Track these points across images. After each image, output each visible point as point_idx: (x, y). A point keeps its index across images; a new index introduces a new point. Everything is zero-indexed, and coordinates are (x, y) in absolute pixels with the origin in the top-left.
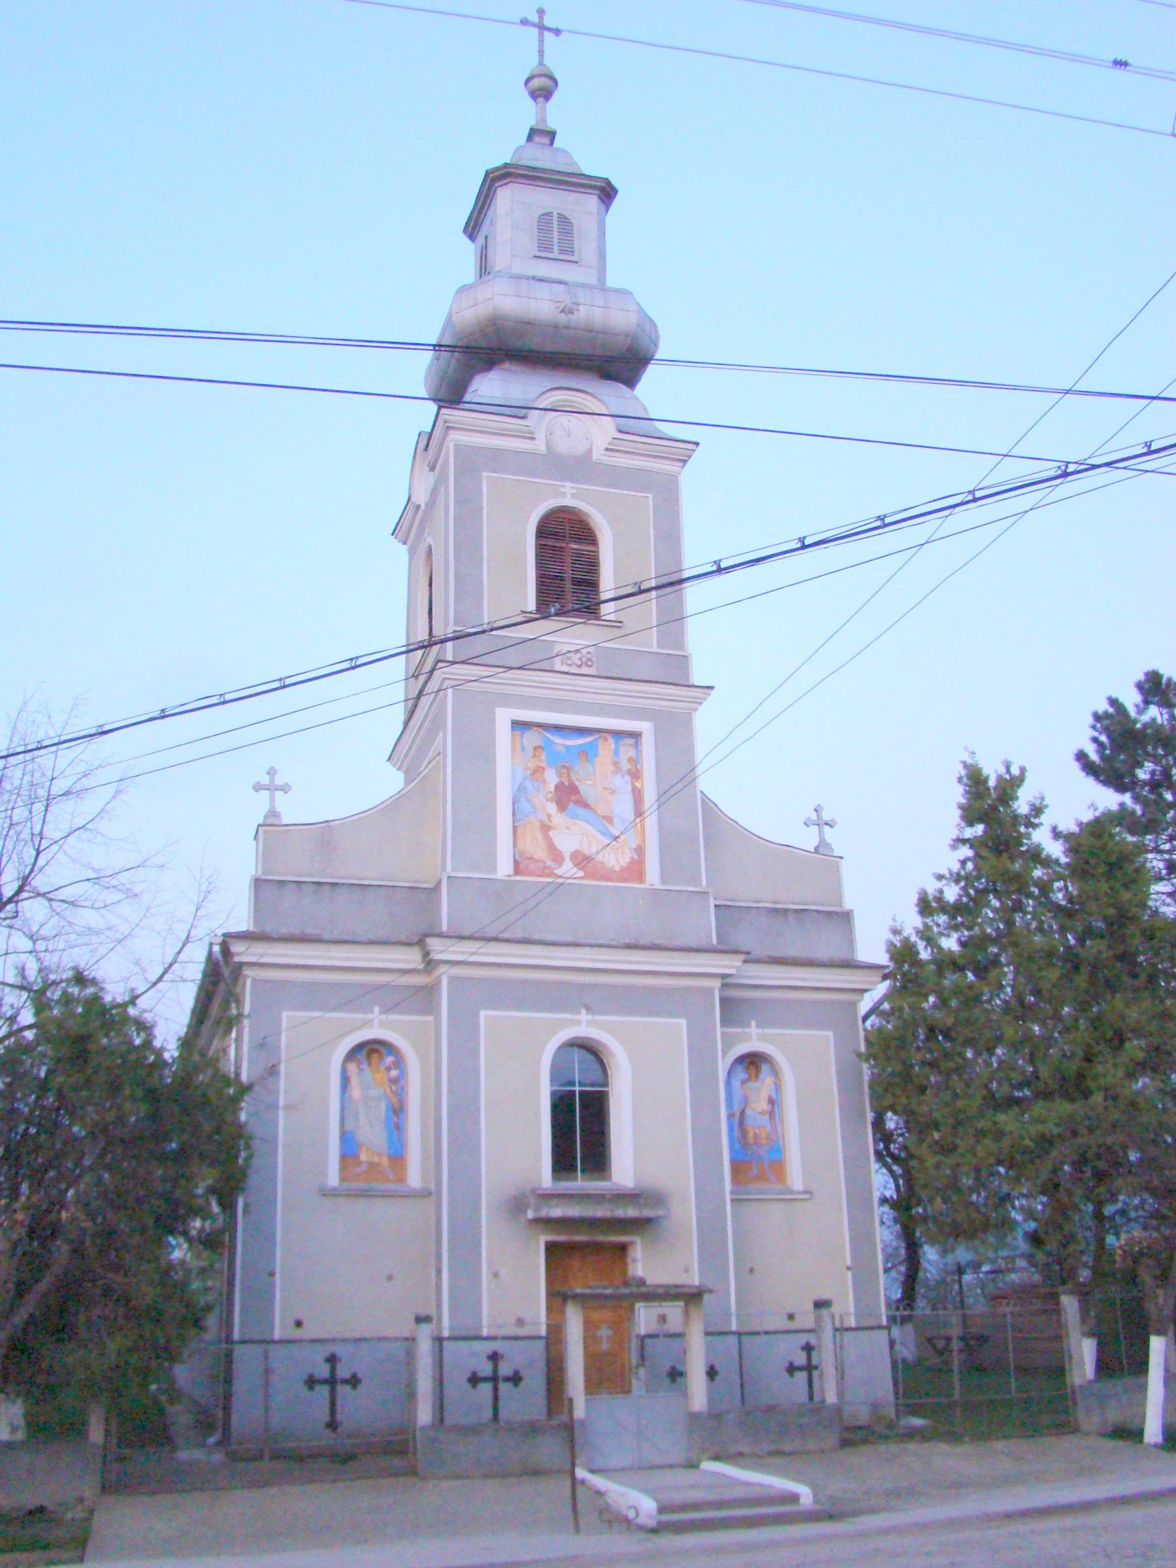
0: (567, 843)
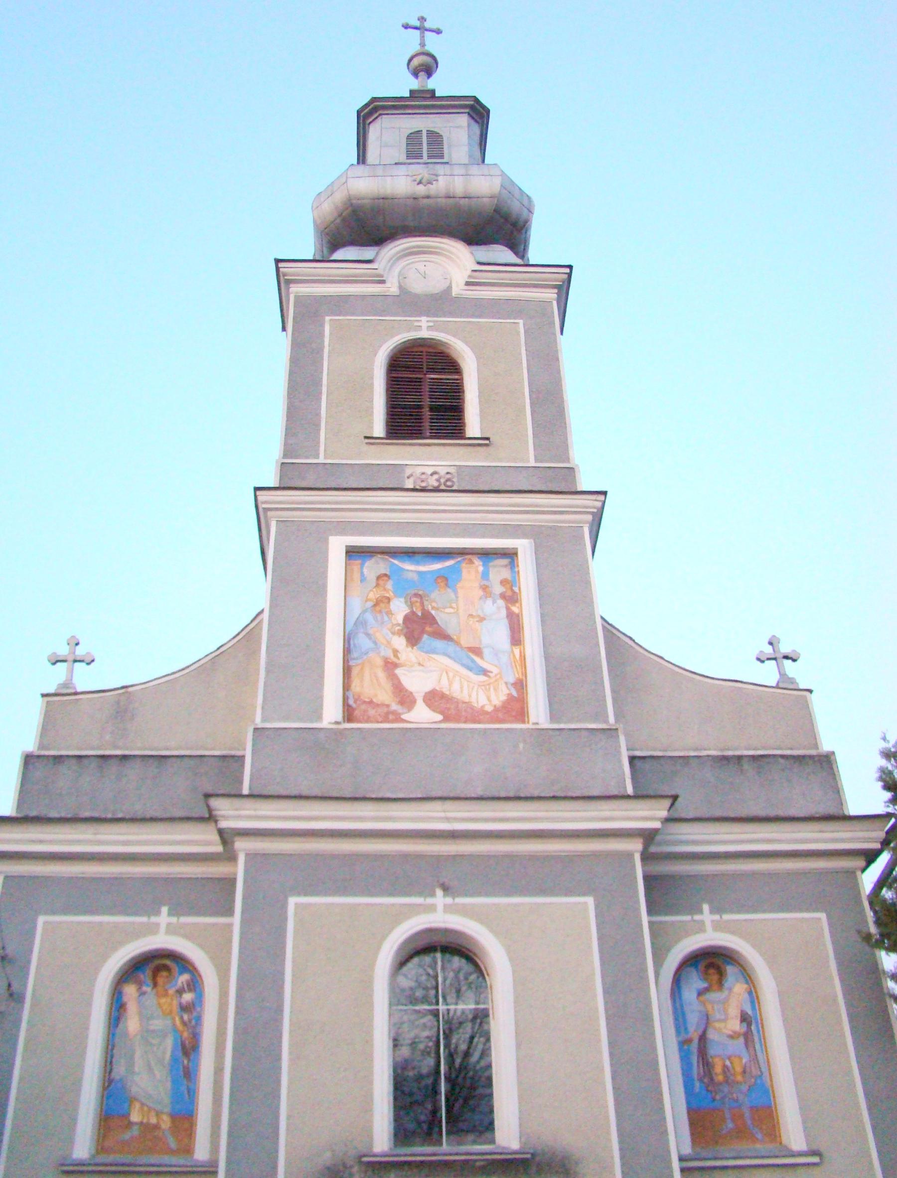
0: (417, 682)
